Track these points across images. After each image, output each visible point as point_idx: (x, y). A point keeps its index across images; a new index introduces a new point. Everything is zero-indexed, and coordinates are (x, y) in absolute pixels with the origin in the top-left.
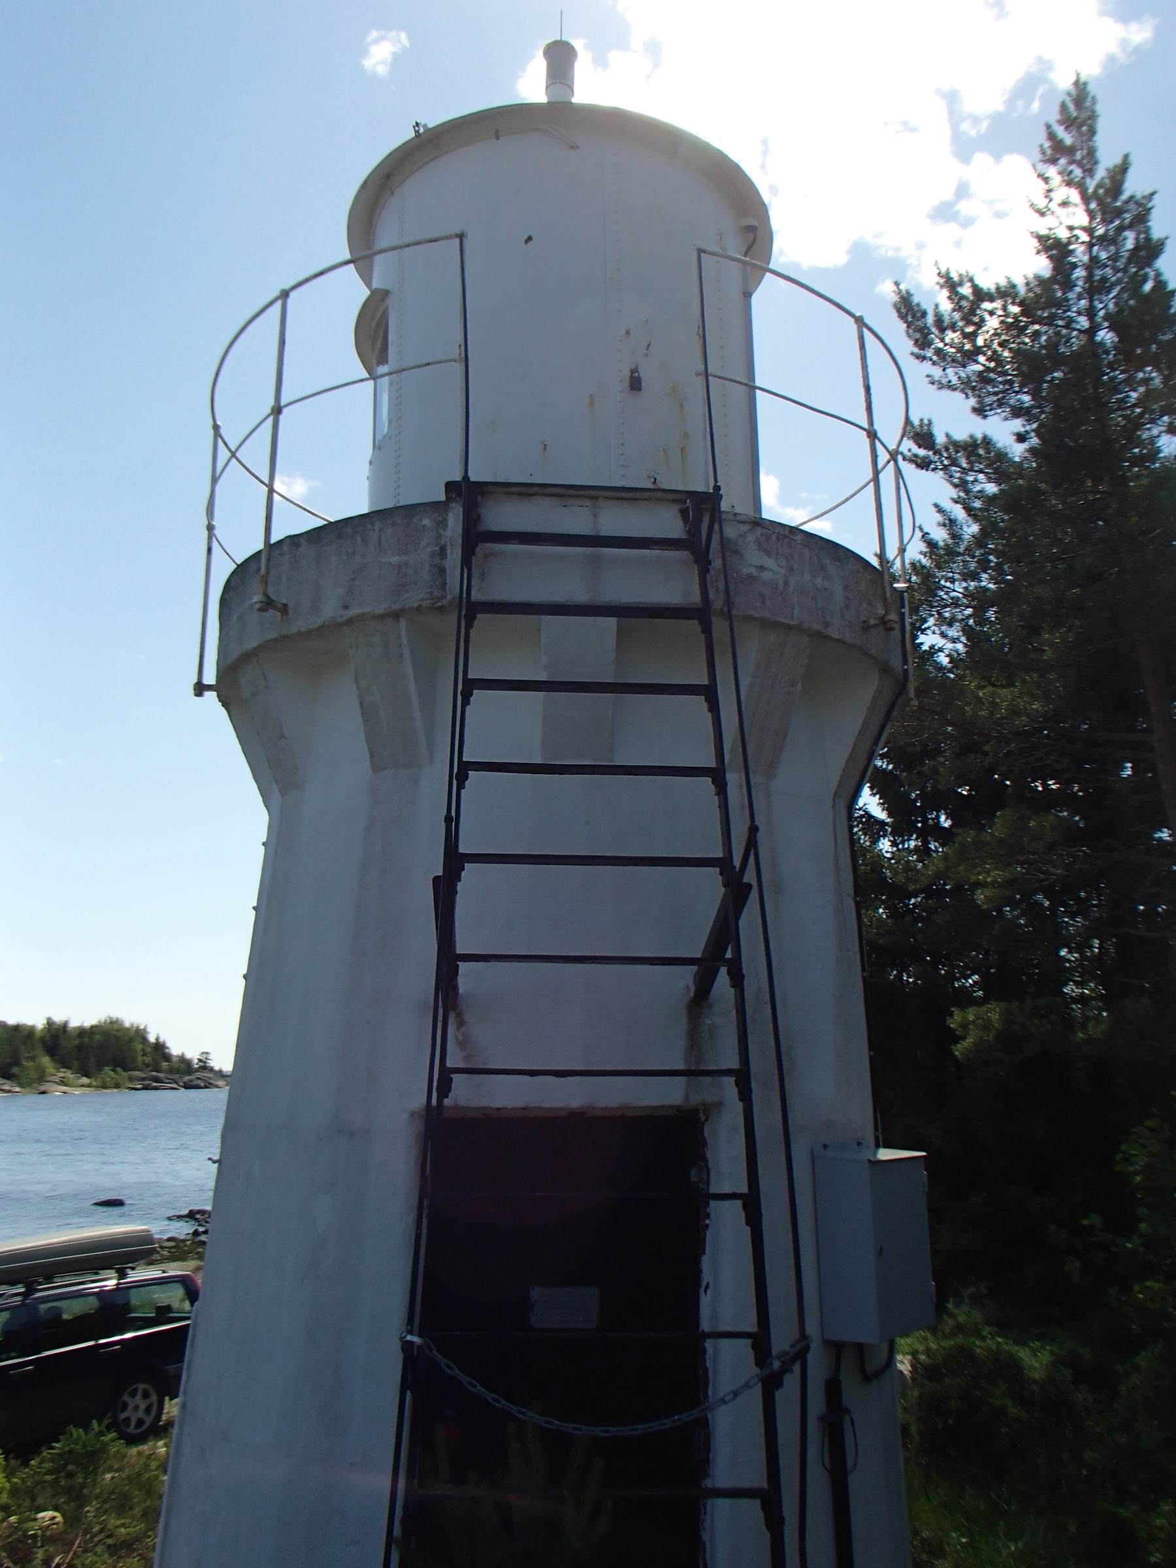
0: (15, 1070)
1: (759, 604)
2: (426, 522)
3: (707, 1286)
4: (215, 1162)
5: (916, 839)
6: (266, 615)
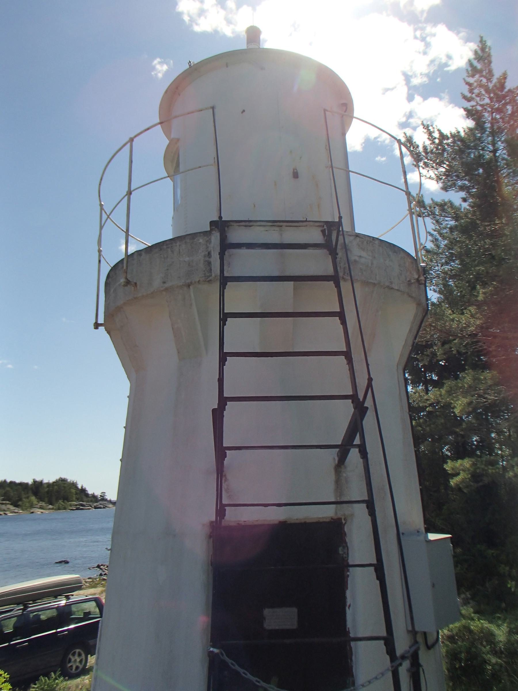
0: (20, 503)
1: (360, 274)
2: (201, 241)
3: (350, 606)
4: (109, 550)
5: (422, 386)
6: (126, 288)
